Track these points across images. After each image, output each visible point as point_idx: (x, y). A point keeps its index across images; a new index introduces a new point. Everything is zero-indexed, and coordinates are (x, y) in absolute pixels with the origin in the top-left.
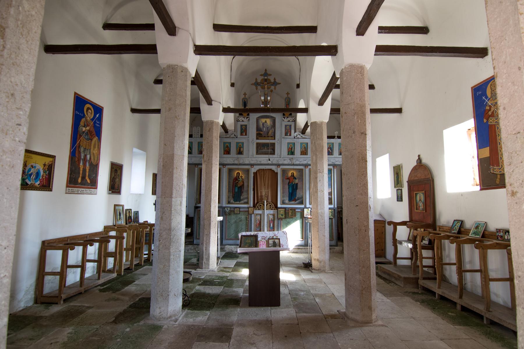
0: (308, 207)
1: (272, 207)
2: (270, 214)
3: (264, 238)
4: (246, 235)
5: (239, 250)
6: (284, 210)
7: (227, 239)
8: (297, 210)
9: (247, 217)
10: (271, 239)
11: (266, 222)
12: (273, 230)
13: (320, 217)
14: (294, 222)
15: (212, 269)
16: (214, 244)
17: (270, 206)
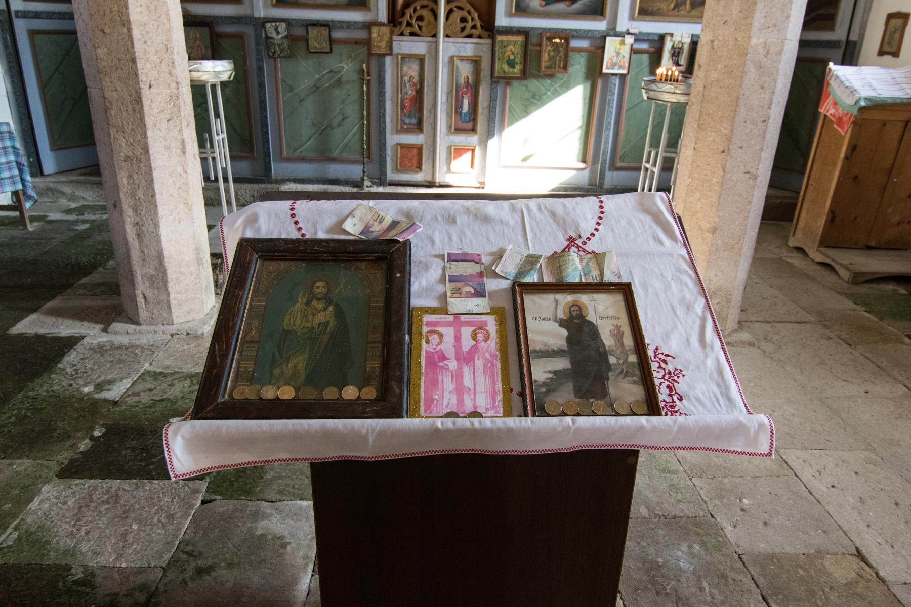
0: (624, 30)
1: (470, 24)
2: (462, 59)
3: (469, 269)
4: (295, 235)
5: (195, 444)
6: (520, 39)
7: (288, 160)
8: (574, 43)
9: (364, 66)
10: (540, 288)
11: (445, 89)
12: (470, 126)
13: (752, 74)
14: (556, 94)
15: (186, 326)
16: (181, 206)
17: (463, 20)
